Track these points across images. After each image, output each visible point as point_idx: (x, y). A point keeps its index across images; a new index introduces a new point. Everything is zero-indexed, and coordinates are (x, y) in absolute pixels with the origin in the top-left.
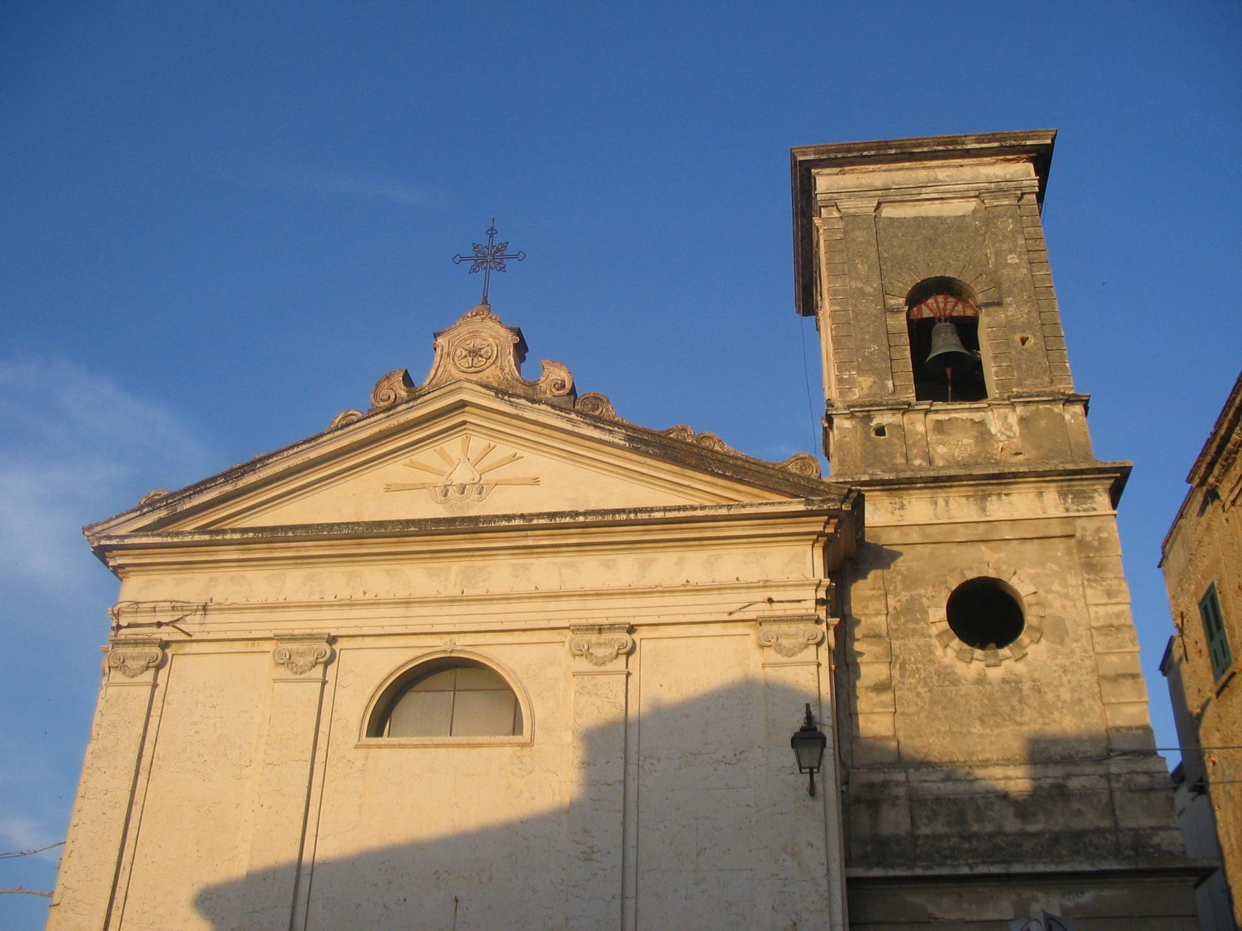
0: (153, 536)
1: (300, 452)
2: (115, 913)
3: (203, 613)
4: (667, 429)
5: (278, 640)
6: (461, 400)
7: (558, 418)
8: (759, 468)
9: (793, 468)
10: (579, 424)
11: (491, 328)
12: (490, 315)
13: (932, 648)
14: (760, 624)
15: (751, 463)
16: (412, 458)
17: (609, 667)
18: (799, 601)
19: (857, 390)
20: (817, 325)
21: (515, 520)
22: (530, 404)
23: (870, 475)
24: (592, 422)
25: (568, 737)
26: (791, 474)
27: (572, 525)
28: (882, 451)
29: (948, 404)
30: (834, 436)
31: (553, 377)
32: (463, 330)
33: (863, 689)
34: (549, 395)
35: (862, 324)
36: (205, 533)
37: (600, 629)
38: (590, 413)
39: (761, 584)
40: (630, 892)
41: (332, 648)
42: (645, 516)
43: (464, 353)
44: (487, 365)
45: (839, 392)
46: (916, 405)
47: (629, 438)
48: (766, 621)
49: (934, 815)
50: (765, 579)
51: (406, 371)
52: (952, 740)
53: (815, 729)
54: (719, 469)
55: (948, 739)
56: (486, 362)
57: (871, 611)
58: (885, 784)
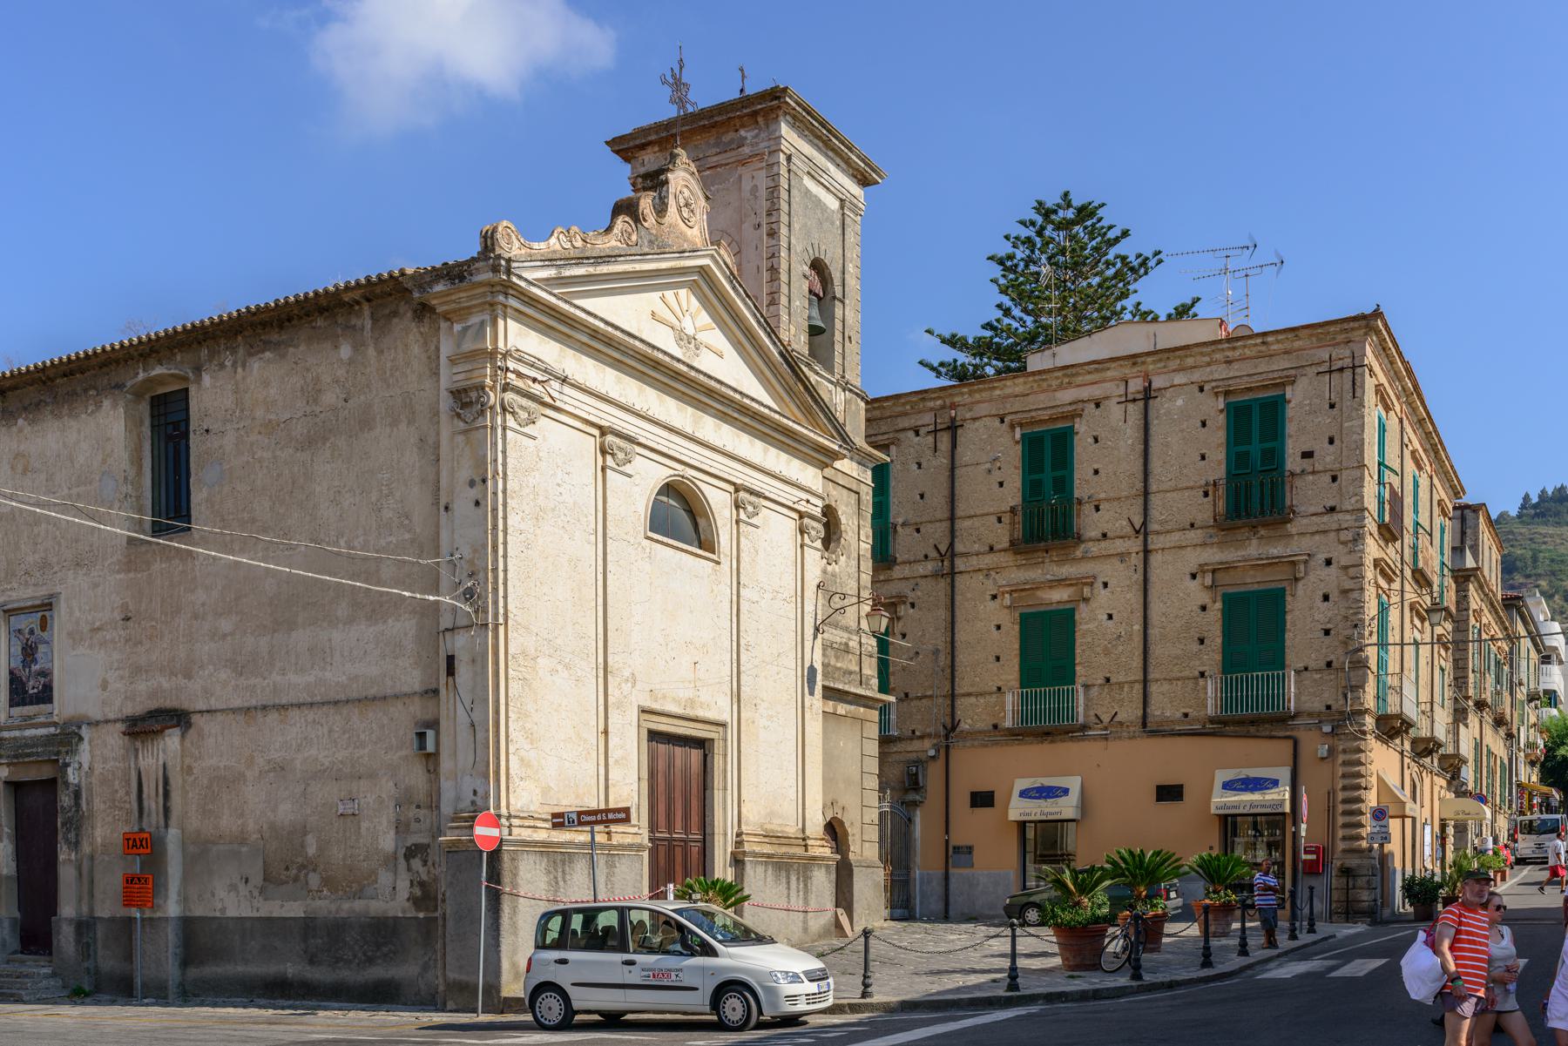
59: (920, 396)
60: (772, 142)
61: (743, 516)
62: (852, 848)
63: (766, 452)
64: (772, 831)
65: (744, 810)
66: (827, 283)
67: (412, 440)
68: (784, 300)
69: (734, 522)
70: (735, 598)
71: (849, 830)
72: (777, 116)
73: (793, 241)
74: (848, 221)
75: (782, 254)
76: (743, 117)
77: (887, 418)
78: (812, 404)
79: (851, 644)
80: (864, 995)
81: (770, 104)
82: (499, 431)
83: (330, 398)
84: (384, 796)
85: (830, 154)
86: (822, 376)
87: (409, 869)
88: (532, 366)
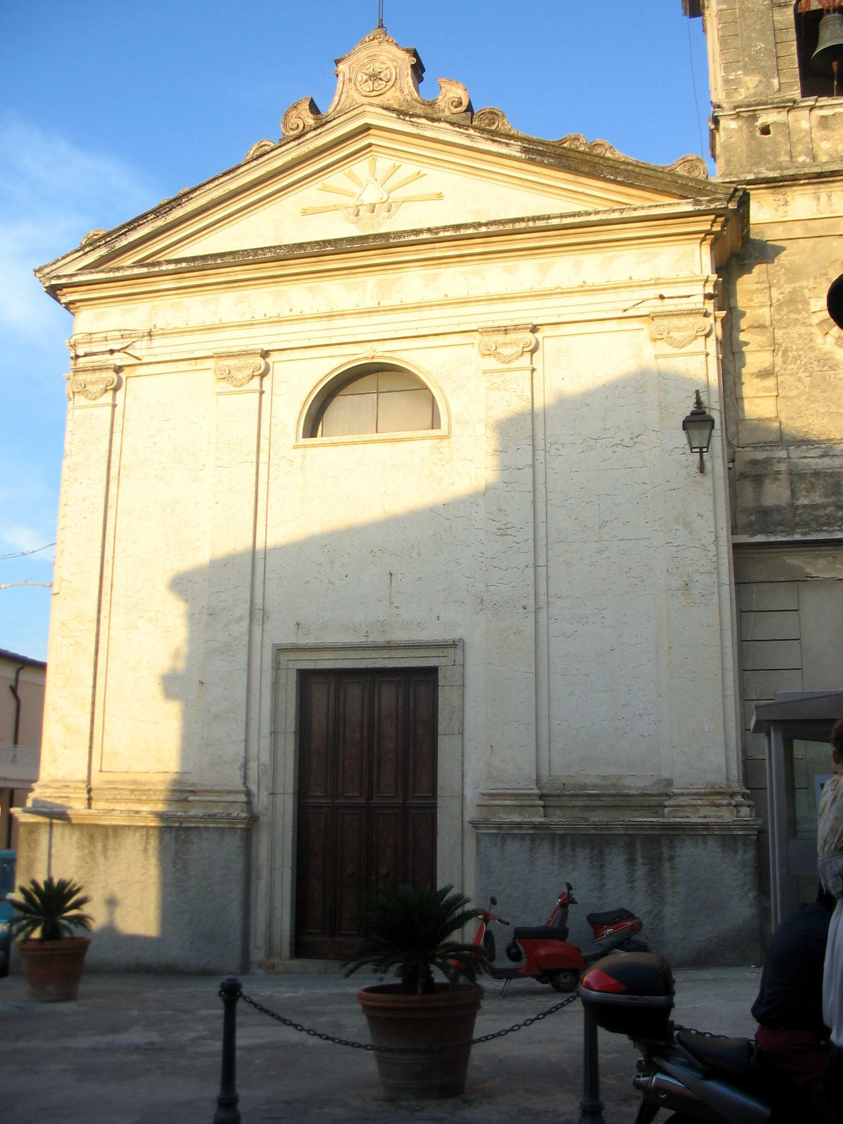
0: (97, 272)
1: (220, 184)
2: (105, 599)
3: (149, 338)
4: (560, 139)
5: (217, 357)
6: (366, 124)
7: (457, 134)
8: (649, 173)
9: (681, 171)
10: (478, 139)
11: (388, 52)
12: (387, 38)
13: (813, 336)
14: (653, 319)
15: (642, 167)
16: (323, 182)
17: (515, 364)
18: (689, 296)
19: (742, 90)
20: (703, 25)
21: (423, 233)
22: (430, 123)
23: (755, 173)
24: (490, 137)
25: (481, 429)
26: (680, 176)
27: (475, 236)
28: (768, 150)
29: (833, 99)
30: (721, 137)
31: (450, 95)
32: (361, 55)
33: (748, 375)
34: (447, 113)
35: (749, 22)
36: (143, 266)
37: (506, 331)
38: (487, 127)
39: (652, 282)
40: (542, 561)
41: (266, 362)
42: (542, 223)
43: (365, 77)
44: (388, 87)
45: (726, 92)
46: (801, 102)
47: (525, 150)
48: (657, 316)
49: (812, 488)
50: (656, 277)
51: (312, 100)
52: (830, 420)
53: (704, 413)
54: (611, 175)
55: (826, 419)
56: (386, 85)
57: (756, 303)
58: (768, 461)
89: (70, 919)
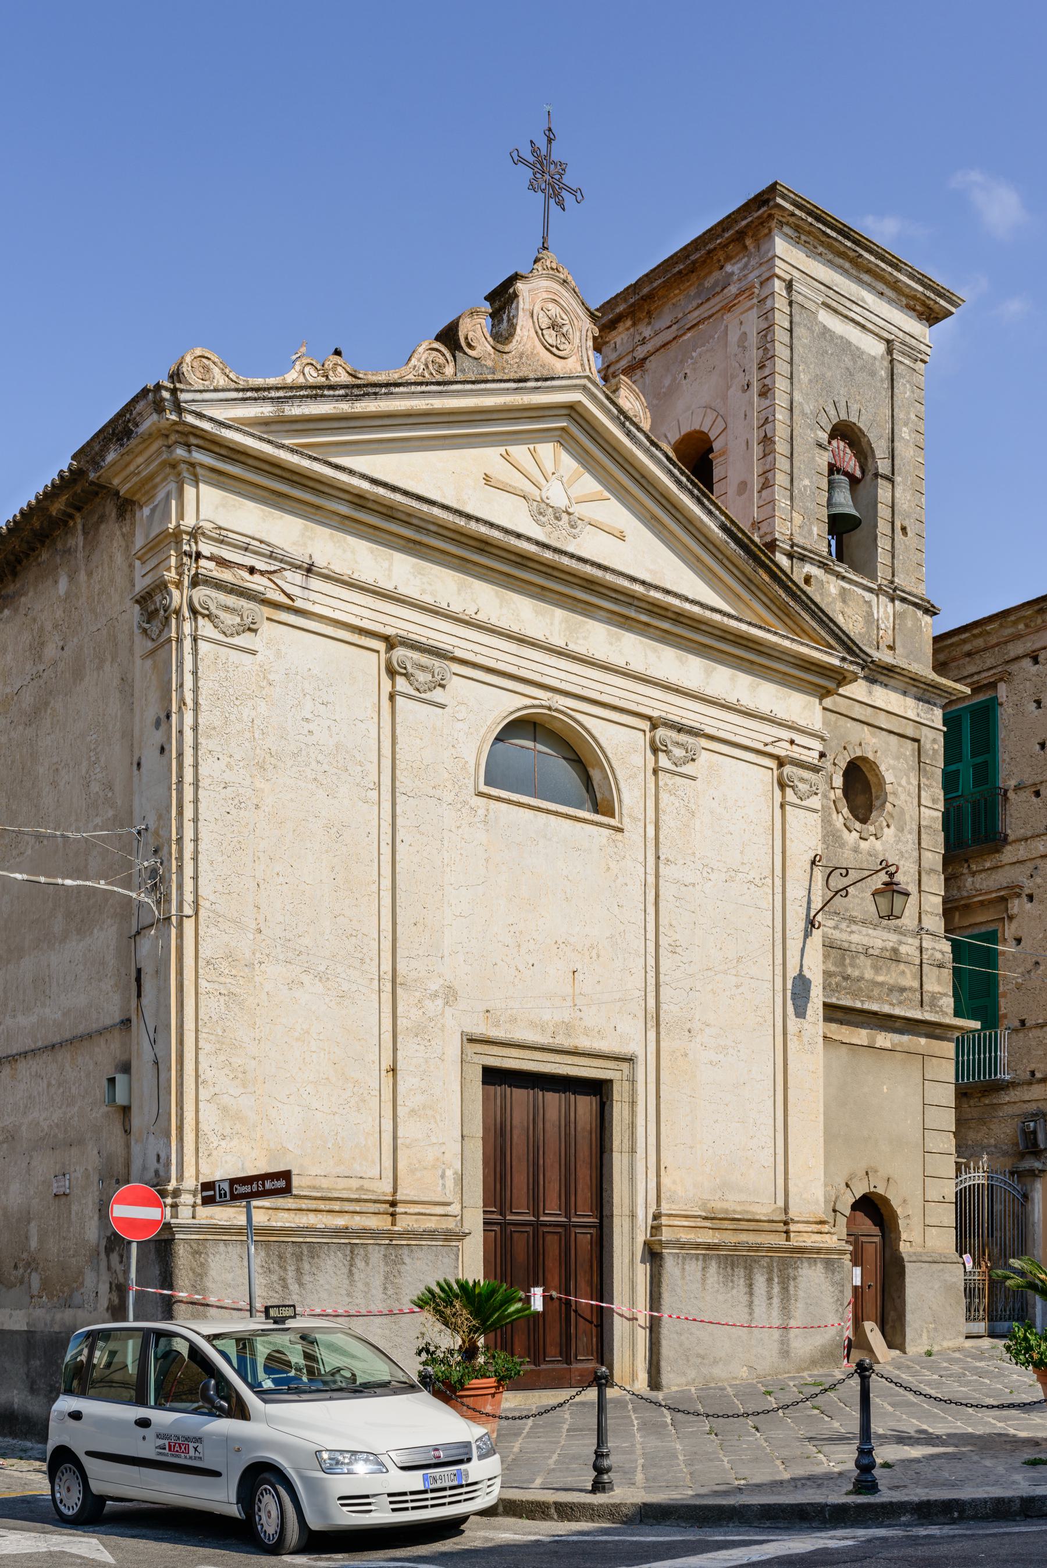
18: (809, 749)
59: (1037, 608)
60: (764, 268)
61: (664, 761)
62: (904, 1236)
63: (708, 673)
64: (726, 1211)
65: (665, 1180)
66: (866, 458)
67: (115, 684)
68: (781, 479)
69: (650, 772)
70: (651, 879)
71: (899, 1211)
72: (770, 231)
73: (797, 397)
74: (899, 369)
75: (778, 416)
76: (726, 245)
77: (993, 647)
78: (788, 599)
79: (903, 949)
80: (598, 1486)
81: (756, 215)
82: (188, 643)
83: (51, 651)
84: (90, 1168)
85: (866, 278)
86: (850, 581)
87: (109, 1268)
88: (246, 549)
89: (82, 1350)
